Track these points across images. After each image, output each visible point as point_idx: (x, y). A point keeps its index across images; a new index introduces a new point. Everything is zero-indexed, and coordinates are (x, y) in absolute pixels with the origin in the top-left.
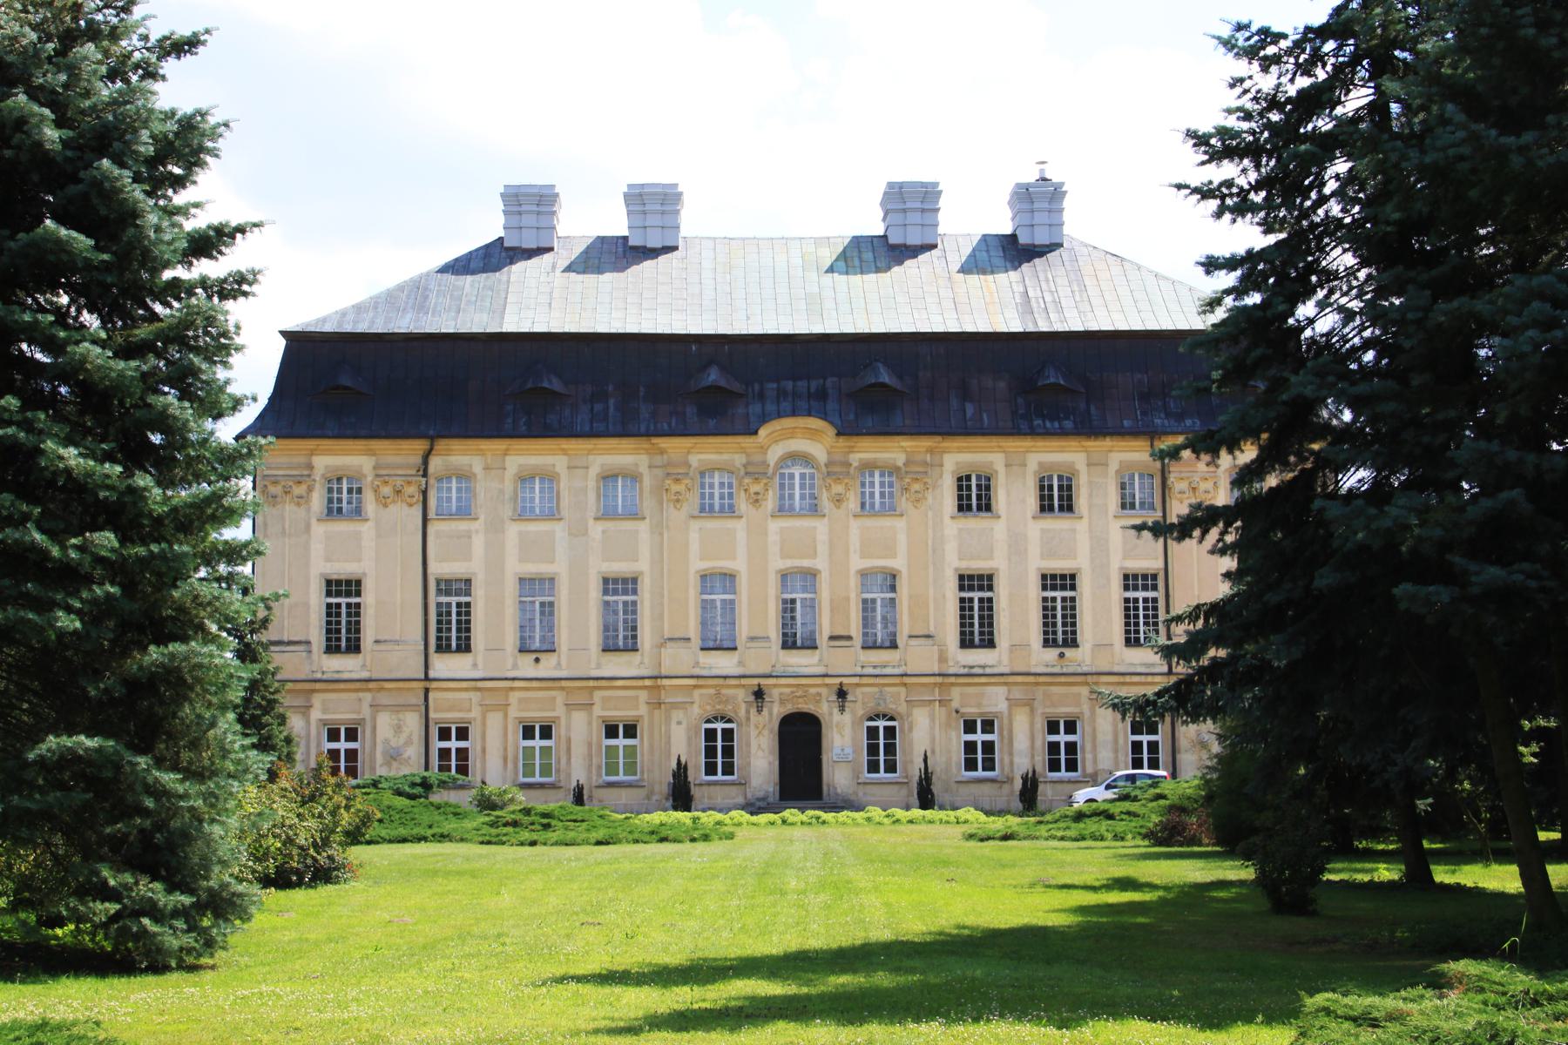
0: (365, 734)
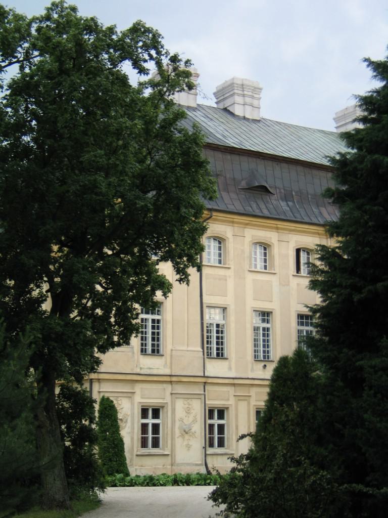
0: (230, 415)
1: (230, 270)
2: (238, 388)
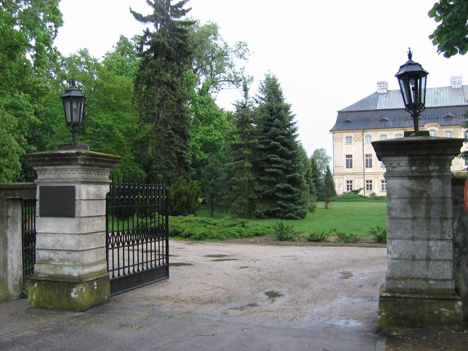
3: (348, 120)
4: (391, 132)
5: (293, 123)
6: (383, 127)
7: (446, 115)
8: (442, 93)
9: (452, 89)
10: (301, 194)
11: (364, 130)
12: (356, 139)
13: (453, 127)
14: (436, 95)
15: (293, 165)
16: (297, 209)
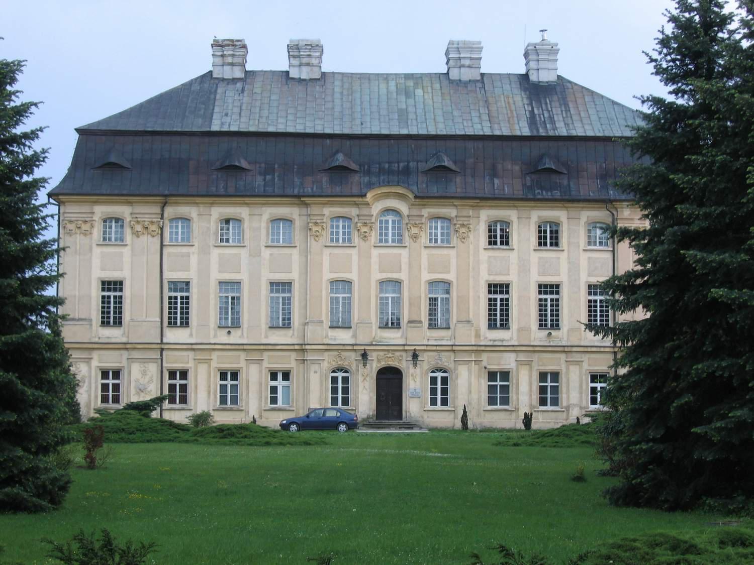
1: (194, 247)
2: (198, 352)
3: (113, 159)
4: (257, 210)
5: (26, 136)
6: (231, 191)
7: (433, 163)
8: (419, 92)
9: (451, 82)
10: (49, 408)
11: (165, 199)
12: (139, 228)
13: (457, 202)
14: (403, 98)
15: (21, 298)
16: (34, 471)
